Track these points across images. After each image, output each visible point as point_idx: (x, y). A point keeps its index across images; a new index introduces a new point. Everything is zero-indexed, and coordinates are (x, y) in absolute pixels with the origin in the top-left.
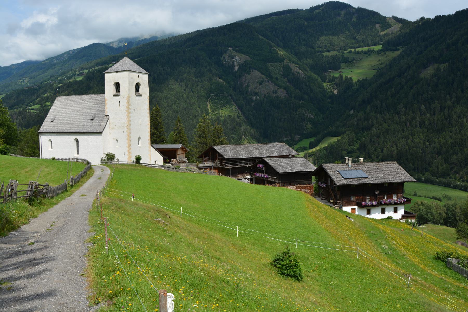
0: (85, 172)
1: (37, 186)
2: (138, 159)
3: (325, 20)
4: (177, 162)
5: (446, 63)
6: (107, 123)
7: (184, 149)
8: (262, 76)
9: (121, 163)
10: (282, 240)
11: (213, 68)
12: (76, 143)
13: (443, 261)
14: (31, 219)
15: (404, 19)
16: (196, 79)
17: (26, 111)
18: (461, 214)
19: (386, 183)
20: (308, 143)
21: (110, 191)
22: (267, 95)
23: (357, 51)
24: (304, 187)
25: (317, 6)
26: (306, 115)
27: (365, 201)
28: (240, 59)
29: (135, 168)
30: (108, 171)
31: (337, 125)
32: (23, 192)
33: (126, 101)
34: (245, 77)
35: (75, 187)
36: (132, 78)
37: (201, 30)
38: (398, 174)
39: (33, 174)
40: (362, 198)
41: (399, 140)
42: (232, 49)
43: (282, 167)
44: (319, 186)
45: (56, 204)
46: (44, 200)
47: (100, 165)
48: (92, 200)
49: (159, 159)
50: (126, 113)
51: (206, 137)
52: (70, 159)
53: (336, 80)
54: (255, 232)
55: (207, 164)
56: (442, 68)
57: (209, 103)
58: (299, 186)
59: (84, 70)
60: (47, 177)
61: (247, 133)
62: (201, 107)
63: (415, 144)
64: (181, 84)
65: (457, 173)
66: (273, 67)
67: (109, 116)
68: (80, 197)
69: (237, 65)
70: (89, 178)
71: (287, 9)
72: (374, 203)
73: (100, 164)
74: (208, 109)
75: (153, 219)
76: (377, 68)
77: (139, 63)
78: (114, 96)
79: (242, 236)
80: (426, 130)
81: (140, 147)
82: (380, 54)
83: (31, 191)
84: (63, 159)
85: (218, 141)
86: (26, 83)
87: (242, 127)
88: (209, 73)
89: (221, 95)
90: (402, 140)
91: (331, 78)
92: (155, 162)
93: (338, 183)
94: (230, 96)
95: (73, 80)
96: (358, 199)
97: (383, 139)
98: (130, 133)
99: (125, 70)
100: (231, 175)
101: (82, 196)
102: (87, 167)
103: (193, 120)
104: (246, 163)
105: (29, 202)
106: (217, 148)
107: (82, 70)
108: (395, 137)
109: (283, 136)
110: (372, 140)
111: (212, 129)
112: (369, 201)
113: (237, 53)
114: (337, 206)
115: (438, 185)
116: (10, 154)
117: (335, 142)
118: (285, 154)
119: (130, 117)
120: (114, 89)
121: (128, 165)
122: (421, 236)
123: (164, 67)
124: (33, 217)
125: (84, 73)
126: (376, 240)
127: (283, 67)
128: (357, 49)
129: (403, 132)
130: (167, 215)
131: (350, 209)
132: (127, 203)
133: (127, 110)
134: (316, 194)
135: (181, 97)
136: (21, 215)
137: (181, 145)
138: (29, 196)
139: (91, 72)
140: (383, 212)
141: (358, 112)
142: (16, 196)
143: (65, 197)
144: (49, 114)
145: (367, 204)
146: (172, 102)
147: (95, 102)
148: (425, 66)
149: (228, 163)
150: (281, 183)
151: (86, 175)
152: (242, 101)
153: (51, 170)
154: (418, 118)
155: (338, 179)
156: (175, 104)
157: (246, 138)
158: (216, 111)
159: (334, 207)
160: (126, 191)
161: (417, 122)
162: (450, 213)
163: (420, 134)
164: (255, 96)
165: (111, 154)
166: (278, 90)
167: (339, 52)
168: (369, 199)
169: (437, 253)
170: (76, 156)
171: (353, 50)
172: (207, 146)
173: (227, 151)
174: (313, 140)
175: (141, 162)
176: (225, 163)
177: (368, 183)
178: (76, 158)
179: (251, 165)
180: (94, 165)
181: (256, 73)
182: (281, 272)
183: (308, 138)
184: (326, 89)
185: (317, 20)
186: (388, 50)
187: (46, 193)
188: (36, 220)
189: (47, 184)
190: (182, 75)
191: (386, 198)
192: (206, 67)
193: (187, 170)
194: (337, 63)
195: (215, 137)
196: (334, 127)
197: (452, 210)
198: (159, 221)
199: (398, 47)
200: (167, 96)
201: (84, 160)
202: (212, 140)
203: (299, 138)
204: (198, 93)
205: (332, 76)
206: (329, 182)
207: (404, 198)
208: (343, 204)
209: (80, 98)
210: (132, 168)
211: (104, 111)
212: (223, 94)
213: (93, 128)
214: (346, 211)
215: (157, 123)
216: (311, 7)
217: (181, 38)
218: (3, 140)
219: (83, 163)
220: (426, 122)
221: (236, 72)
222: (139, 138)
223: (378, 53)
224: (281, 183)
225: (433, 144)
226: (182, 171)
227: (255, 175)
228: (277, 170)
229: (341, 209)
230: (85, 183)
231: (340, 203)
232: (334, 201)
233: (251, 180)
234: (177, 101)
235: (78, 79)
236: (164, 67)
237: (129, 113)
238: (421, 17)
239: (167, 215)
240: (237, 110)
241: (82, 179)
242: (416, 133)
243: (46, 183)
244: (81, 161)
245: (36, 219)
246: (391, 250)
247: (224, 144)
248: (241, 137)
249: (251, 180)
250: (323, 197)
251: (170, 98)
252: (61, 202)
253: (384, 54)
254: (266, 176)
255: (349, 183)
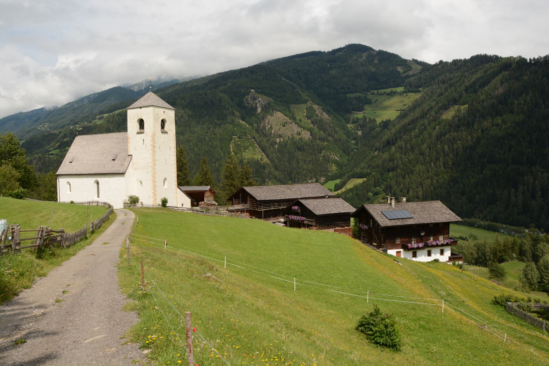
0: (107, 217)
1: (49, 232)
2: (164, 202)
3: (347, 63)
4: (206, 205)
5: (465, 104)
6: (129, 163)
7: (213, 191)
8: (286, 117)
9: (146, 207)
10: (347, 293)
11: (235, 110)
12: (96, 185)
13: (502, 305)
14: (37, 278)
15: (424, 62)
16: (218, 122)
17: (46, 156)
18: (491, 254)
19: (432, 223)
20: (334, 185)
21: (137, 238)
22: (291, 137)
23: (380, 92)
24: (342, 229)
25: (339, 49)
26: (331, 156)
27: (411, 243)
28: (262, 101)
29: (162, 212)
30: (133, 216)
31: (362, 166)
32: (30, 241)
33: (151, 139)
34: (269, 119)
35: (96, 234)
36: (157, 114)
37: (223, 73)
38: (443, 213)
39: (48, 219)
40: (407, 240)
41: (424, 180)
42: (254, 91)
43: (318, 208)
44: (360, 228)
45: (73, 255)
46: (58, 250)
47: (123, 209)
48: (117, 249)
49: (187, 202)
50: (151, 152)
51: (233, 179)
52: (90, 203)
53: (360, 121)
54: (314, 284)
55: (237, 207)
56: (462, 109)
57: (232, 146)
58: (337, 228)
59: (104, 114)
60: (65, 223)
61: (271, 175)
62: (224, 149)
63: (440, 184)
64: (203, 126)
65: (481, 213)
66: (296, 108)
67: (132, 155)
68: (103, 245)
69: (260, 107)
70: (111, 223)
71: (309, 51)
72: (421, 245)
73: (122, 207)
74: (231, 152)
75: (200, 274)
76: (400, 109)
77: (163, 98)
78: (138, 133)
79: (300, 289)
80: (450, 170)
81: (166, 189)
82: (403, 96)
83: (41, 238)
84: (82, 203)
85: (247, 182)
86: (44, 127)
87: (266, 170)
88: (231, 115)
89: (243, 137)
90: (427, 180)
91: (355, 119)
92: (182, 205)
93: (383, 224)
94: (253, 138)
95: (93, 124)
96: (403, 241)
97: (408, 180)
98: (155, 173)
99: (150, 105)
100: (264, 219)
101: (105, 244)
102: (109, 210)
103: (215, 163)
104: (280, 205)
105: (38, 252)
106: (248, 189)
107: (102, 114)
108: (420, 178)
109: (308, 178)
110: (398, 182)
111: (240, 170)
112: (415, 243)
113: (260, 95)
114: (381, 249)
115: (463, 225)
116: (26, 198)
117: (360, 184)
118: (320, 195)
119: (155, 156)
120: (137, 126)
121: (153, 208)
122: (473, 279)
123: (185, 110)
124: (40, 276)
125: (104, 116)
126: (431, 286)
127: (307, 109)
128: (380, 91)
129: (428, 173)
130: (213, 267)
131: (396, 252)
132: (163, 253)
133: (151, 149)
134: (357, 235)
135: (203, 140)
136: (22, 275)
137: (210, 186)
138: (39, 246)
139: (111, 116)
140: (429, 254)
141: (383, 154)
142: (19, 246)
143: (85, 246)
144: (68, 154)
145: (413, 247)
146: (194, 145)
147: (117, 141)
148: (446, 108)
149: (260, 205)
150: (318, 226)
151: (108, 220)
152: (265, 143)
153: (69, 215)
154: (441, 158)
155: (382, 220)
156: (197, 147)
157: (271, 181)
158: (239, 153)
159: (379, 250)
160: (155, 238)
161: (441, 163)
162: (480, 252)
163: (445, 175)
164: (278, 138)
165: (134, 196)
166: (301, 132)
167: (362, 94)
168: (415, 241)
169: (495, 298)
170: (96, 199)
171: (375, 92)
172: (234, 187)
173: (259, 193)
174: (338, 181)
175: (167, 205)
176: (257, 205)
177: (414, 223)
178: (96, 201)
179: (285, 207)
180: (116, 209)
181: (279, 114)
182: (374, 341)
183: (333, 180)
184: (350, 131)
185: (339, 62)
186: (409, 92)
187: (61, 241)
188: (44, 279)
189: (62, 230)
190: (204, 118)
191: (432, 239)
192: (228, 109)
193: (217, 213)
194: (361, 104)
195: (242, 178)
196: (359, 168)
197: (482, 250)
198: (209, 277)
199: (419, 89)
200: (188, 139)
201: (106, 204)
202: (240, 181)
203: (324, 180)
204: (220, 135)
205: (356, 117)
206: (371, 223)
207: (450, 239)
208: (388, 247)
209: (100, 137)
210: (158, 211)
211: (127, 150)
212: (246, 136)
213: (115, 169)
214: (391, 255)
215: (182, 164)
216: (333, 49)
217: (202, 80)
218: (19, 183)
219: (104, 207)
220: (450, 163)
221: (260, 114)
222: (165, 179)
223: (400, 95)
224: (318, 226)
225: (457, 184)
226: (213, 214)
227: (289, 218)
228: (314, 212)
229: (385, 253)
230: (107, 228)
231: (385, 246)
232: (377, 243)
233: (285, 223)
234: (199, 143)
235: (98, 123)
236: (185, 110)
237: (154, 152)
238: (439, 60)
239: (213, 267)
240: (261, 153)
241: (103, 225)
242: (440, 173)
243: (61, 229)
244: (102, 205)
245: (45, 278)
246: (448, 297)
247: (253, 185)
248: (265, 180)
249: (285, 223)
250: (364, 240)
251: (191, 141)
252: (80, 252)
253: (406, 95)
254: (302, 219)
255: (395, 224)
